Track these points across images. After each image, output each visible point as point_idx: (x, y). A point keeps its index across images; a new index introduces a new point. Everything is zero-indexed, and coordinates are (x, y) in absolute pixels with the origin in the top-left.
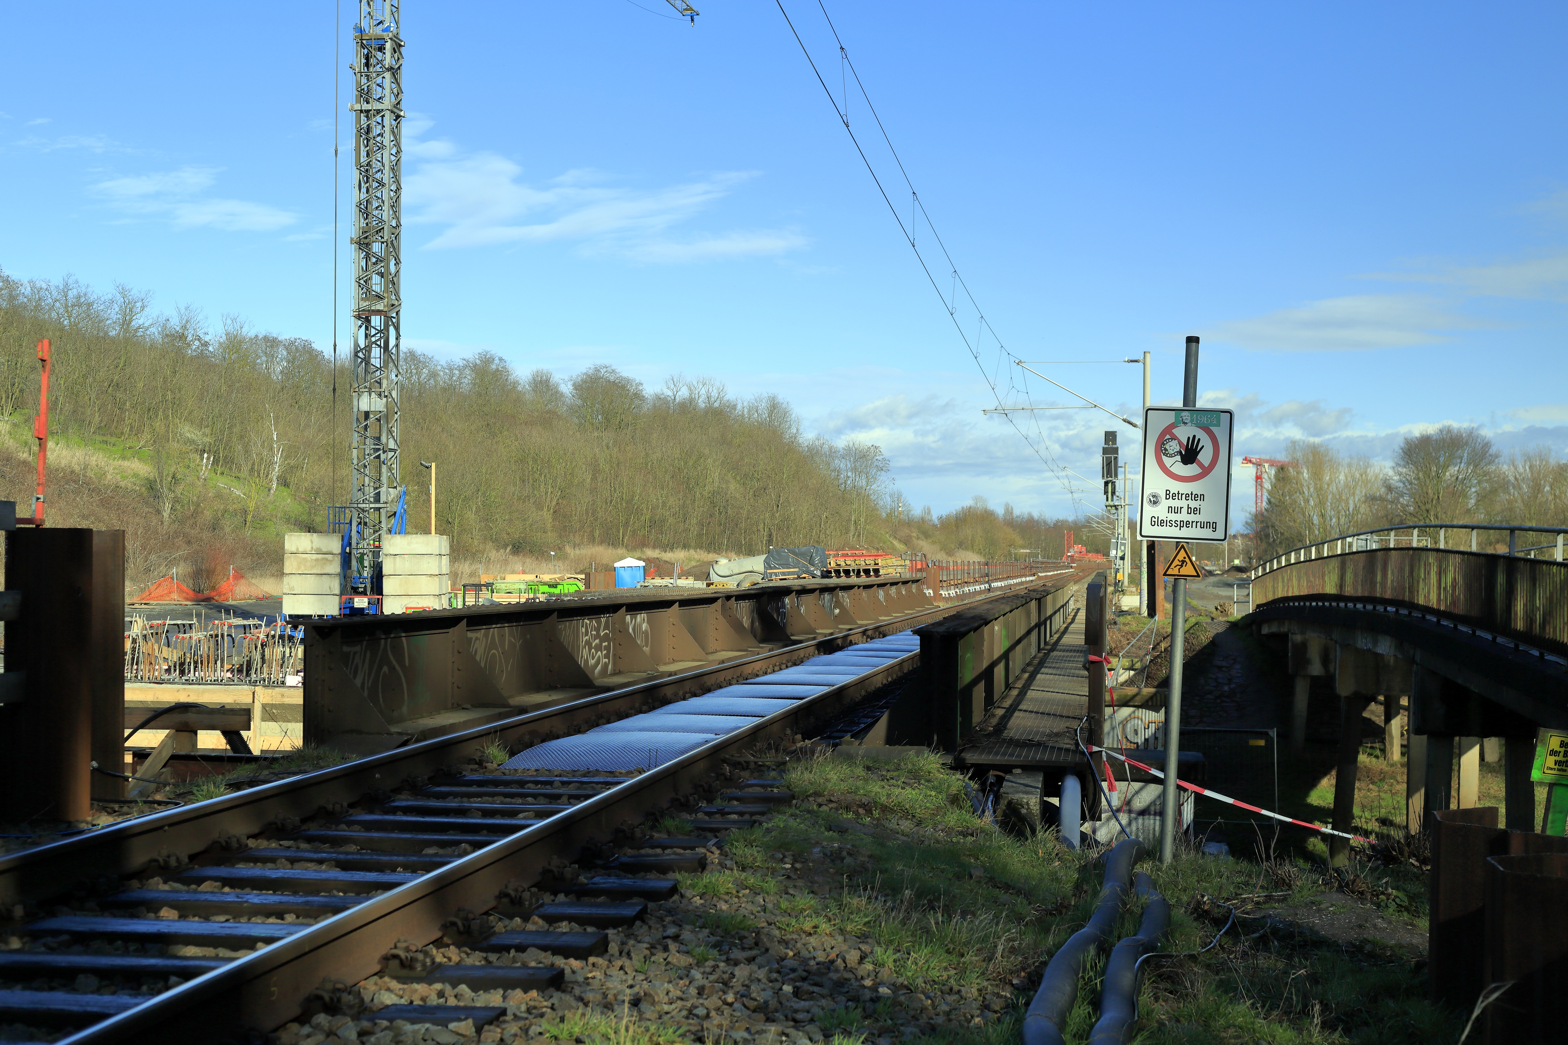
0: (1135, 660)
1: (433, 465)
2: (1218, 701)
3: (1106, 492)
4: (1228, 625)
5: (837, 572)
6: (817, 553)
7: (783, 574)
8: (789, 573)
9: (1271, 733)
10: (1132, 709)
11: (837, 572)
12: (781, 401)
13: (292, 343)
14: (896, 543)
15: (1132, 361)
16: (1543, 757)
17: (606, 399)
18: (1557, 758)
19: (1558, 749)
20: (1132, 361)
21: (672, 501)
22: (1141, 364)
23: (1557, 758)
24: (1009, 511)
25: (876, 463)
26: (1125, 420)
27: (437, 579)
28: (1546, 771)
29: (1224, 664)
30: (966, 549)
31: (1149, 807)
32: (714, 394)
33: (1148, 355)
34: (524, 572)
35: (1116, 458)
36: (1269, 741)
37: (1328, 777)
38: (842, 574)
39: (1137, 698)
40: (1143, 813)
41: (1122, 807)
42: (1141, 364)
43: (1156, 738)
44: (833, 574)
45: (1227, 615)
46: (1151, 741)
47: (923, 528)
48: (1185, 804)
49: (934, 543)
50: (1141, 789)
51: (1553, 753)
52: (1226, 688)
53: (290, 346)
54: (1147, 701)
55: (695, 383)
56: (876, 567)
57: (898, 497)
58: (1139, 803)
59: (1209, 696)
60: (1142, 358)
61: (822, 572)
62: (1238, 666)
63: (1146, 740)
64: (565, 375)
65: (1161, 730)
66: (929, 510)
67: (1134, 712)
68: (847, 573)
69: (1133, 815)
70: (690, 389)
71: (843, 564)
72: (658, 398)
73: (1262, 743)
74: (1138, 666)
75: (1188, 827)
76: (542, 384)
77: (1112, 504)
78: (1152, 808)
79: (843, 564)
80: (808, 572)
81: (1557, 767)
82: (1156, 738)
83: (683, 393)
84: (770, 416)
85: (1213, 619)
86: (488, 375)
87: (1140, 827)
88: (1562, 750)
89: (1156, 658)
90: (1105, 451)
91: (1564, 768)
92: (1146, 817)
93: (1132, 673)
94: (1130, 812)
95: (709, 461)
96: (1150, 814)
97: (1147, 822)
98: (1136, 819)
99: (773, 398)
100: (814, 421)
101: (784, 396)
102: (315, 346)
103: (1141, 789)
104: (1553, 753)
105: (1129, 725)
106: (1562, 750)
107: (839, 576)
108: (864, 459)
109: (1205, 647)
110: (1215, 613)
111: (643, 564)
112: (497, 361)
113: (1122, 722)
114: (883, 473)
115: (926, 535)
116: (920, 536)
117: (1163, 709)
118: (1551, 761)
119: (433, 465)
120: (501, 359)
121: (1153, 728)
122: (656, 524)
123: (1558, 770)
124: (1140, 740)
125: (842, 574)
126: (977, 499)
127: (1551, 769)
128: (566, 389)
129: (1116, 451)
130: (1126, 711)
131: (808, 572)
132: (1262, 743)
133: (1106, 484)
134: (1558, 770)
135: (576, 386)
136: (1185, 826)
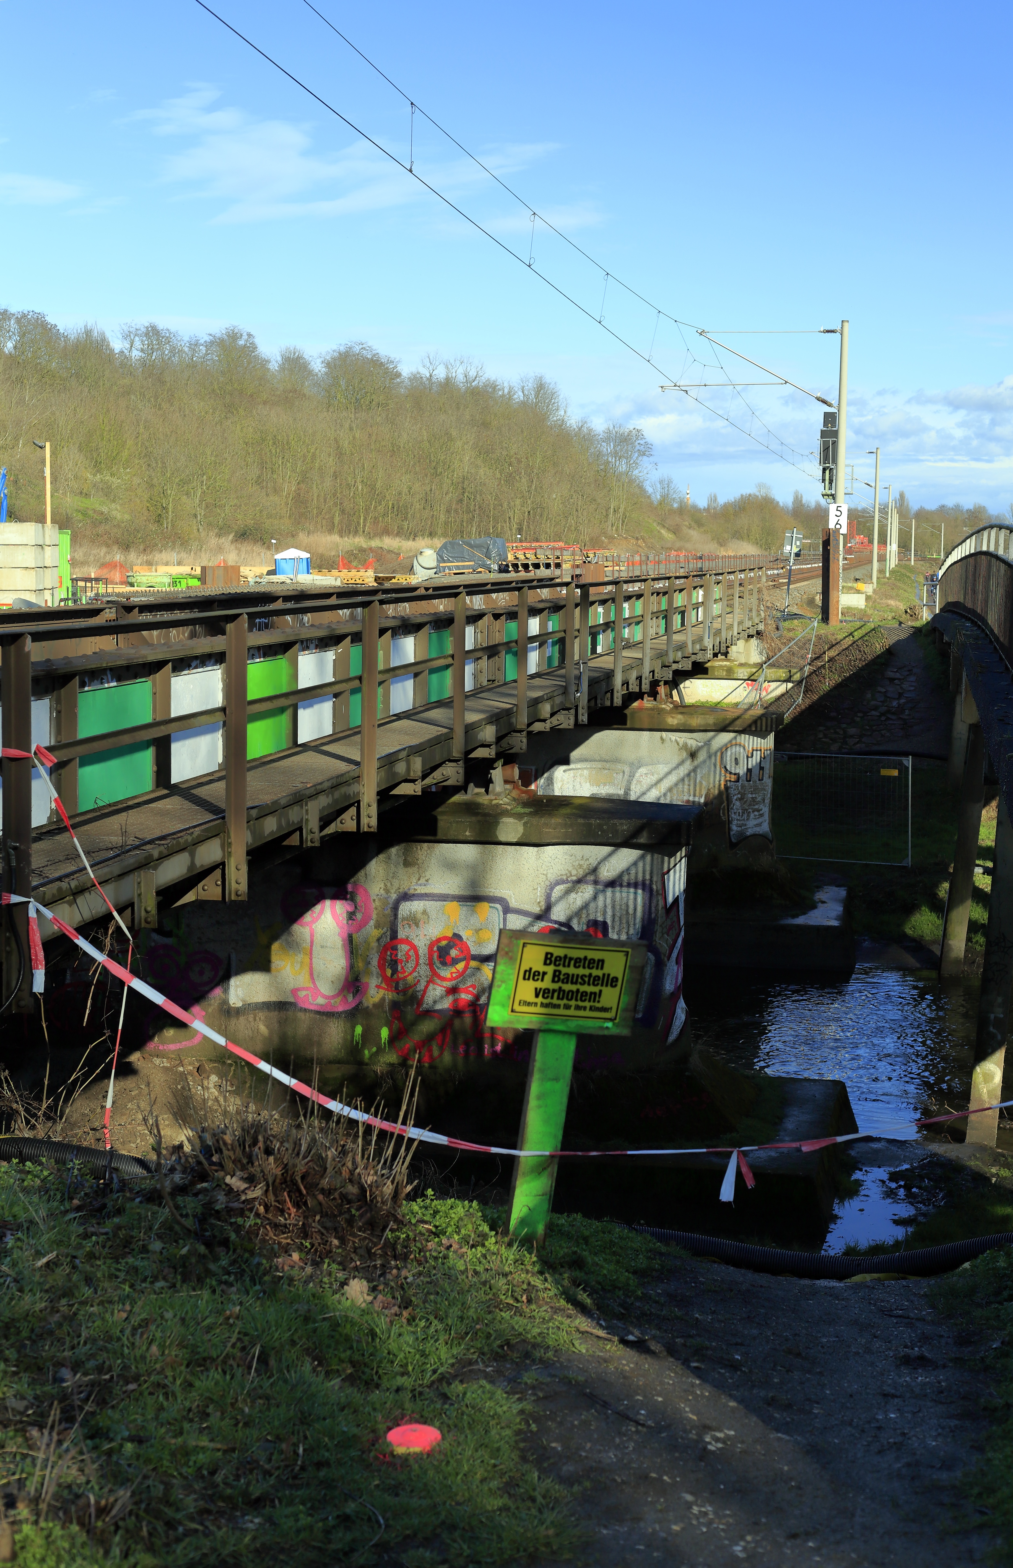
0: (793, 671)
1: (48, 445)
2: (883, 718)
3: (824, 480)
4: (912, 631)
5: (515, 566)
6: (494, 545)
7: (458, 567)
8: (464, 567)
9: (905, 763)
10: (732, 735)
11: (515, 566)
12: (548, 381)
13: (24, 316)
14: (663, 531)
15: (828, 331)
16: (512, 984)
17: (360, 379)
18: (539, 985)
19: (541, 968)
20: (828, 331)
21: (417, 487)
22: (838, 335)
23: (539, 985)
24: (798, 500)
25: (638, 447)
26: (818, 399)
27: (33, 572)
28: (517, 1007)
29: (898, 675)
30: (742, 538)
31: (621, 875)
32: (472, 374)
33: (846, 324)
34: (179, 563)
35: (834, 443)
36: (903, 770)
37: (987, 808)
38: (520, 568)
39: (738, 722)
40: (611, 884)
41: (586, 876)
42: (838, 335)
43: (762, 768)
44: (511, 569)
45: (917, 619)
46: (756, 772)
47: (697, 517)
48: (672, 872)
49: (706, 532)
50: (610, 855)
51: (530, 975)
52: (895, 703)
53: (22, 319)
54: (750, 726)
55: (452, 361)
56: (557, 561)
57: (666, 483)
58: (608, 872)
59: (874, 713)
60: (839, 328)
61: (500, 566)
62: (912, 678)
63: (749, 771)
64: (317, 351)
65: (768, 759)
66: (715, 497)
67: (735, 738)
68: (526, 567)
69: (600, 887)
70: (447, 368)
71: (522, 557)
72: (416, 378)
73: (895, 773)
74: (797, 677)
75: (676, 900)
76: (295, 364)
77: (829, 492)
78: (625, 878)
79: (522, 557)
80: (484, 566)
81: (540, 1000)
82: (762, 768)
83: (440, 374)
84: (537, 397)
85: (901, 623)
86: (234, 351)
87: (609, 901)
88: (550, 969)
89: (819, 668)
90: (824, 434)
91: (555, 1001)
92: (618, 889)
93: (790, 685)
94: (596, 882)
95: (459, 443)
96: (621, 886)
97: (618, 895)
98: (603, 891)
99: (541, 378)
100: (587, 403)
101: (550, 377)
102: (51, 319)
103: (610, 855)
104: (530, 975)
105: (729, 753)
106: (550, 969)
107: (517, 571)
108: (627, 442)
109: (878, 657)
110: (904, 617)
111: (308, 555)
112: (245, 337)
113: (721, 749)
114: (645, 458)
115: (699, 523)
116: (693, 524)
117: (395, 792)
118: (527, 990)
119: (48, 445)
120: (249, 335)
121: (757, 758)
122: (401, 511)
123: (542, 1005)
124: (741, 770)
125: (520, 568)
126: (760, 486)
127: (529, 1004)
128: (318, 367)
129: (835, 434)
130: (725, 737)
131: (484, 566)
132: (895, 773)
133: (824, 470)
134: (542, 1005)
135: (328, 365)
136: (670, 899)
